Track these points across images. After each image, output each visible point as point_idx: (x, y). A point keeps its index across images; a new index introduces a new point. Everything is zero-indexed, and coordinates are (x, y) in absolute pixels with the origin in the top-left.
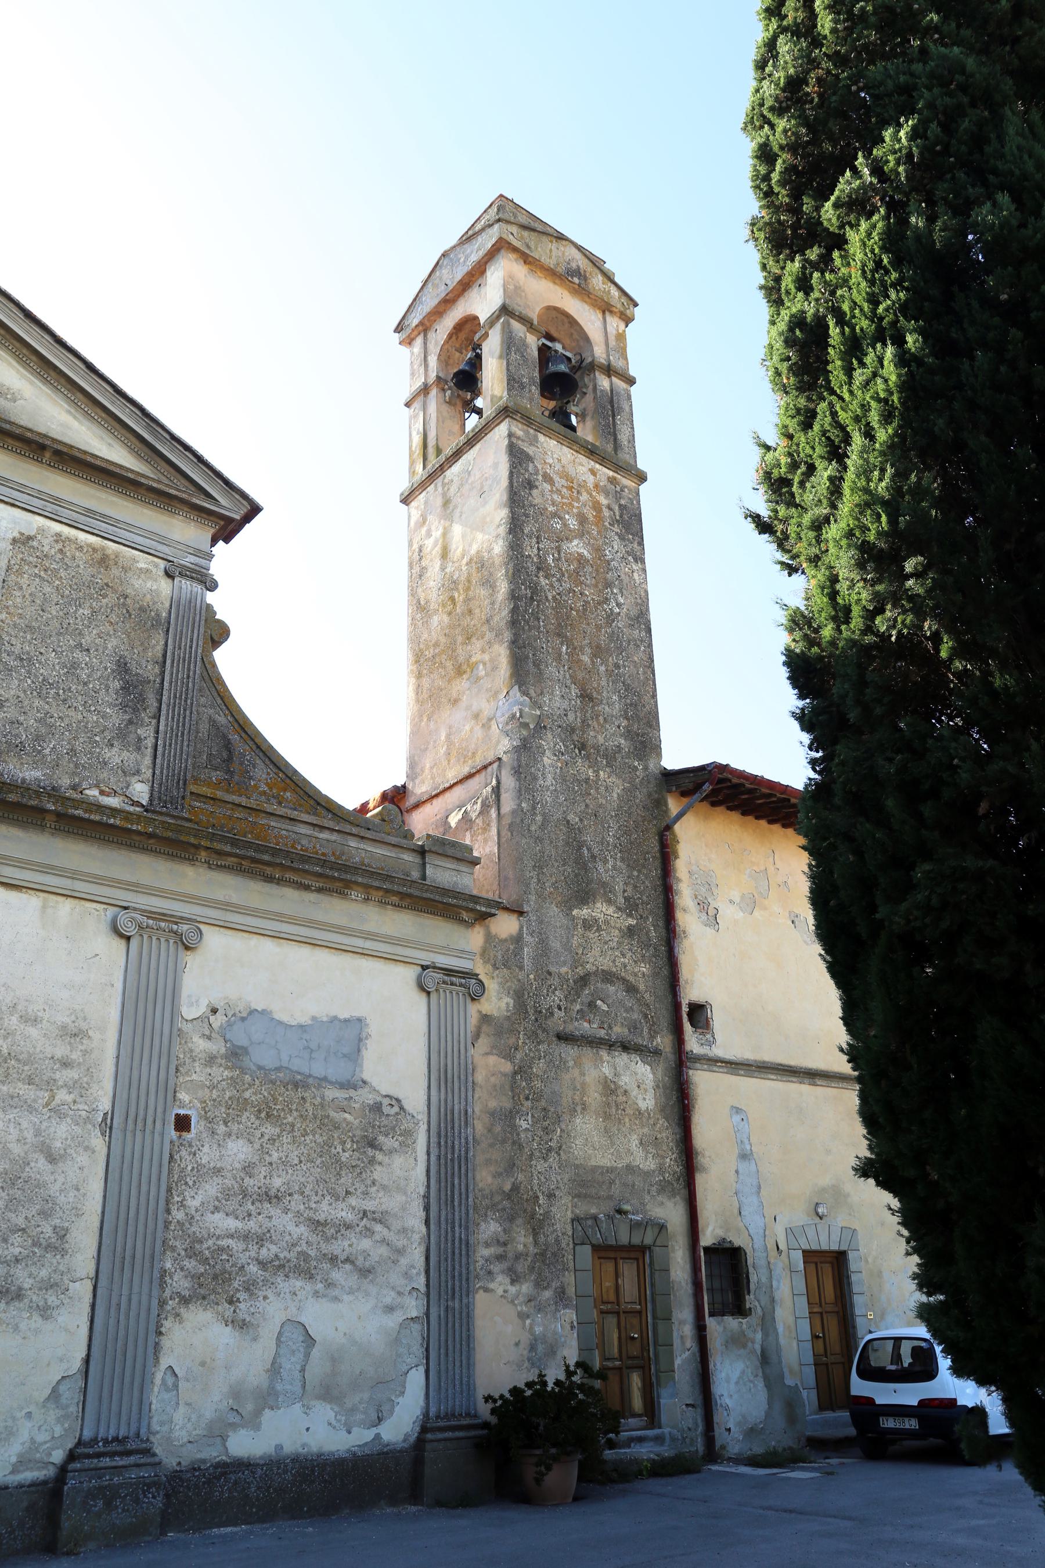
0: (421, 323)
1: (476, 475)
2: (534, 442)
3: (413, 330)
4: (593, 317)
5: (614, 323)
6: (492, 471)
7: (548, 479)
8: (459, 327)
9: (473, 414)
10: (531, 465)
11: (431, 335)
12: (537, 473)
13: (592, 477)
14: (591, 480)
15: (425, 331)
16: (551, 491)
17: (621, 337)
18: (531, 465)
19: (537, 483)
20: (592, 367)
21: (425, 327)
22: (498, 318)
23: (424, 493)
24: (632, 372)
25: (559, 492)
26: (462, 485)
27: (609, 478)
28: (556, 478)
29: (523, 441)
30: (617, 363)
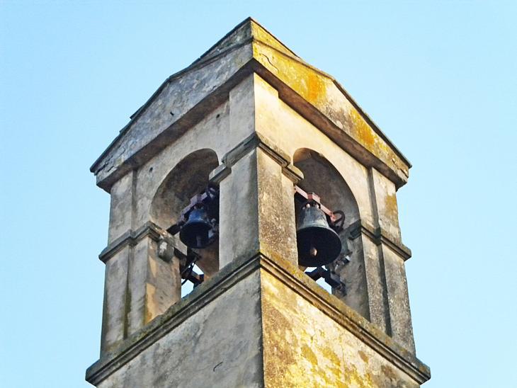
0: (132, 160)
1: (208, 341)
2: (290, 305)
3: (119, 168)
4: (357, 172)
5: (383, 185)
6: (232, 336)
7: (307, 352)
8: (183, 166)
9: (188, 281)
10: (287, 332)
11: (142, 175)
12: (295, 344)
13: (362, 362)
14: (360, 364)
15: (136, 170)
16: (314, 370)
17: (392, 202)
18: (287, 332)
19: (296, 358)
20: (358, 229)
21: (135, 164)
22: (246, 150)
23: (124, 369)
24: (406, 242)
25: (322, 372)
26: (185, 356)
27: (383, 367)
28: (319, 355)
29: (278, 300)
30: (389, 230)
